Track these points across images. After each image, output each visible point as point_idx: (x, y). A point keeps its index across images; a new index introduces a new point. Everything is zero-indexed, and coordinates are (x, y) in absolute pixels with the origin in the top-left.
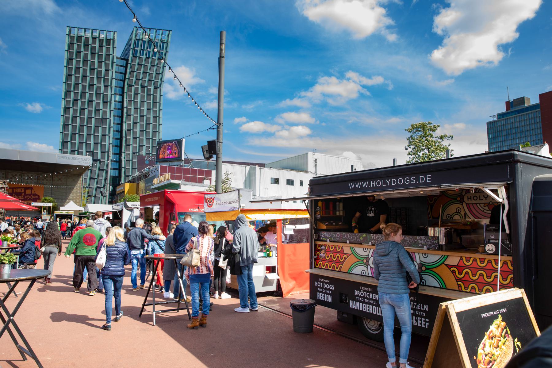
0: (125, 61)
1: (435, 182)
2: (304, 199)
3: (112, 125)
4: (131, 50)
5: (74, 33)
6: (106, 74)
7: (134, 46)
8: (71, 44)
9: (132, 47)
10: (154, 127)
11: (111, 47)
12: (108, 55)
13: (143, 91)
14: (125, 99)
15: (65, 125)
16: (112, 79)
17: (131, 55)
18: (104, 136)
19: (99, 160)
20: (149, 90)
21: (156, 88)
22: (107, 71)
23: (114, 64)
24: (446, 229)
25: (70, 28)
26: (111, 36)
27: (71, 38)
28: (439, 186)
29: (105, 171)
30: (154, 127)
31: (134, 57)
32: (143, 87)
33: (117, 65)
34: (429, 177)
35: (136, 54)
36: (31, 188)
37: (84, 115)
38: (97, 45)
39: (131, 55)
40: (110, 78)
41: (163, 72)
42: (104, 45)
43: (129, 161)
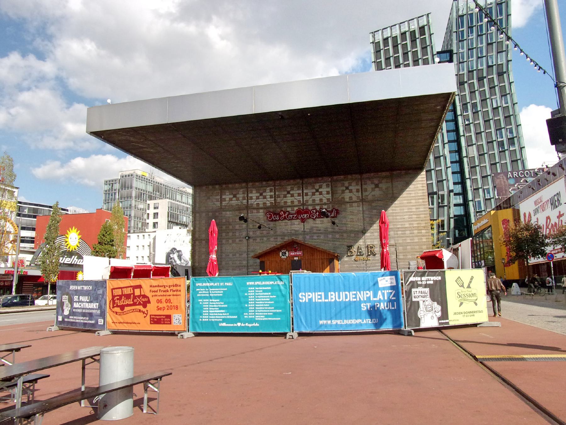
0: (448, 54)
1: (265, 317)
3: (449, 164)
4: (454, 35)
7: (458, 27)
8: (377, 52)
9: (454, 30)
11: (427, 36)
12: (424, 48)
16: (447, 168)
17: (455, 41)
19: (435, 193)
20: (491, 81)
25: (373, 33)
26: (423, 22)
27: (376, 45)
29: (446, 208)
31: (460, 41)
34: (353, 294)
35: (463, 36)
36: (140, 287)
38: (408, 41)
39: (455, 41)
42: (417, 36)
43: (487, 176)
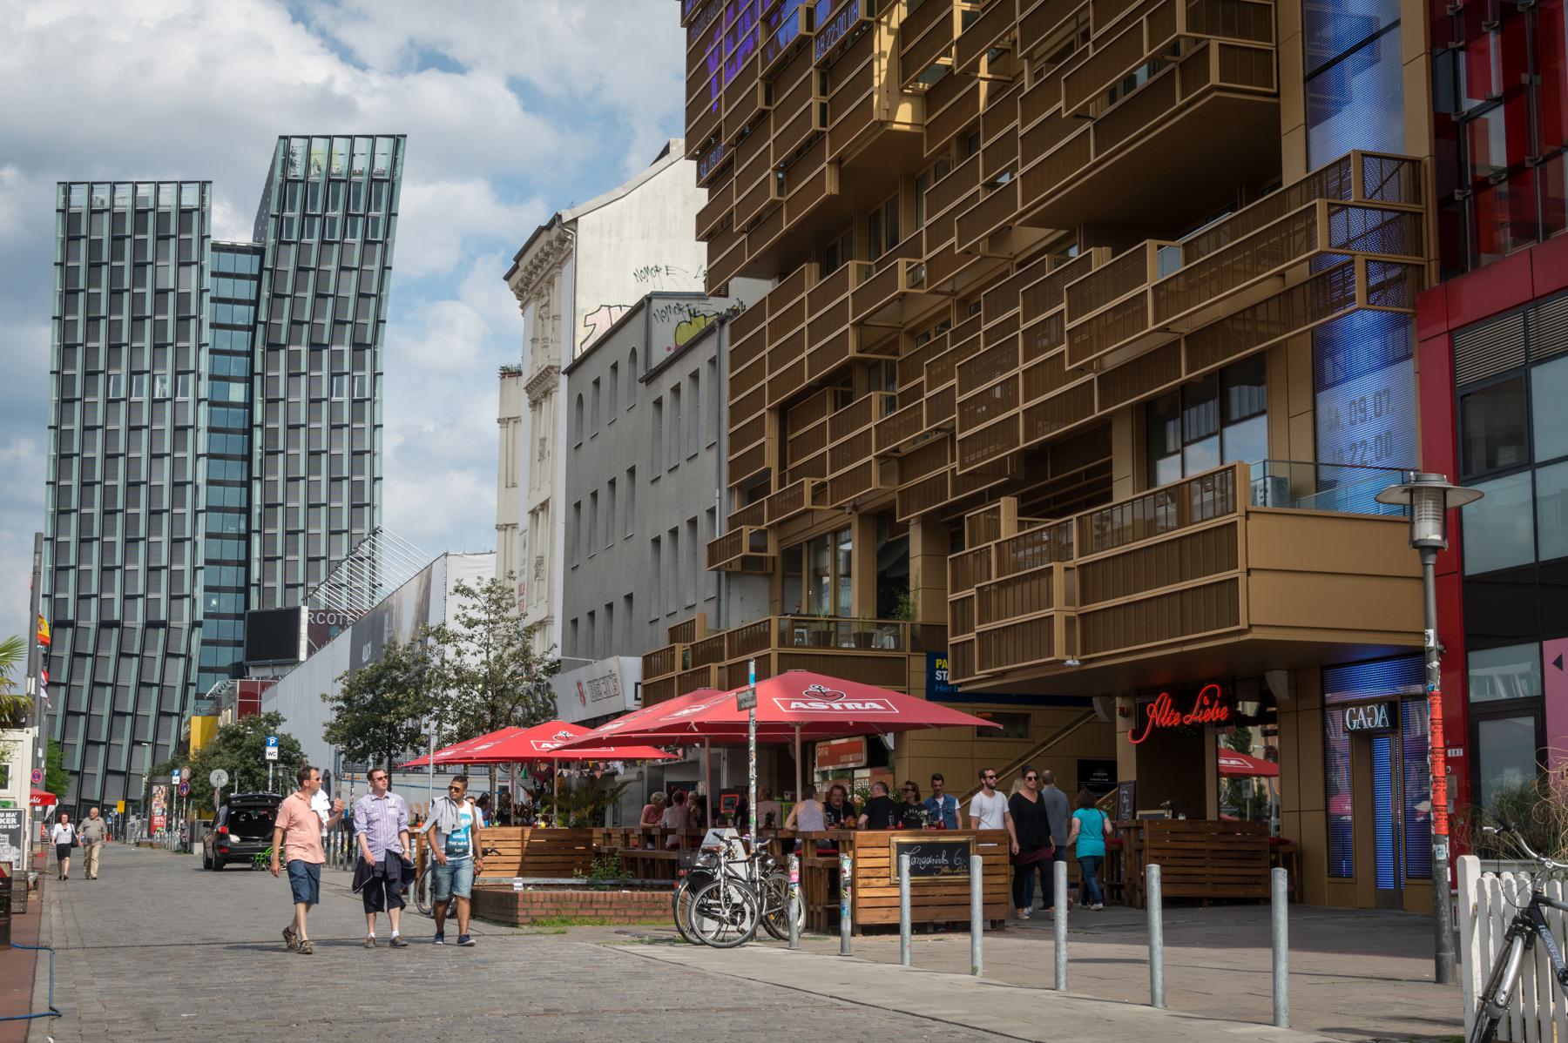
2: (238, 644)
5: (79, 198)
6: (182, 334)
10: (357, 488)
13: (315, 364)
14: (258, 397)
15: (66, 346)
18: (176, 542)
21: (358, 347)
22: (183, 320)
23: (207, 297)
24: (1162, 866)
25: (67, 188)
26: (190, 198)
27: (70, 219)
28: (863, 704)
30: (357, 488)
32: (316, 347)
33: (213, 300)
37: (166, 313)
40: (192, 343)
41: (381, 288)
